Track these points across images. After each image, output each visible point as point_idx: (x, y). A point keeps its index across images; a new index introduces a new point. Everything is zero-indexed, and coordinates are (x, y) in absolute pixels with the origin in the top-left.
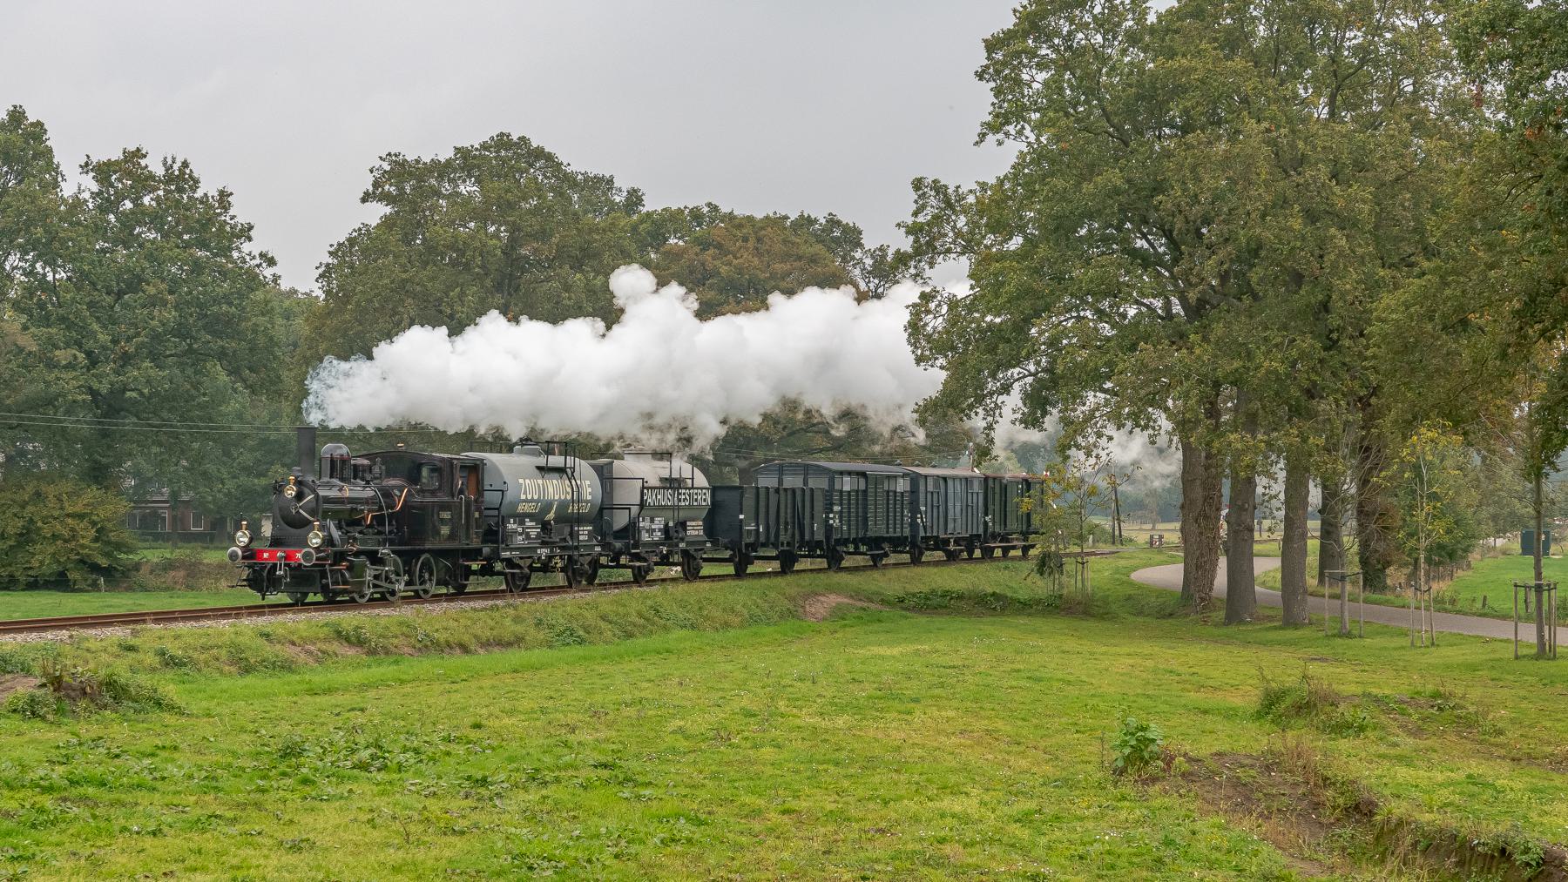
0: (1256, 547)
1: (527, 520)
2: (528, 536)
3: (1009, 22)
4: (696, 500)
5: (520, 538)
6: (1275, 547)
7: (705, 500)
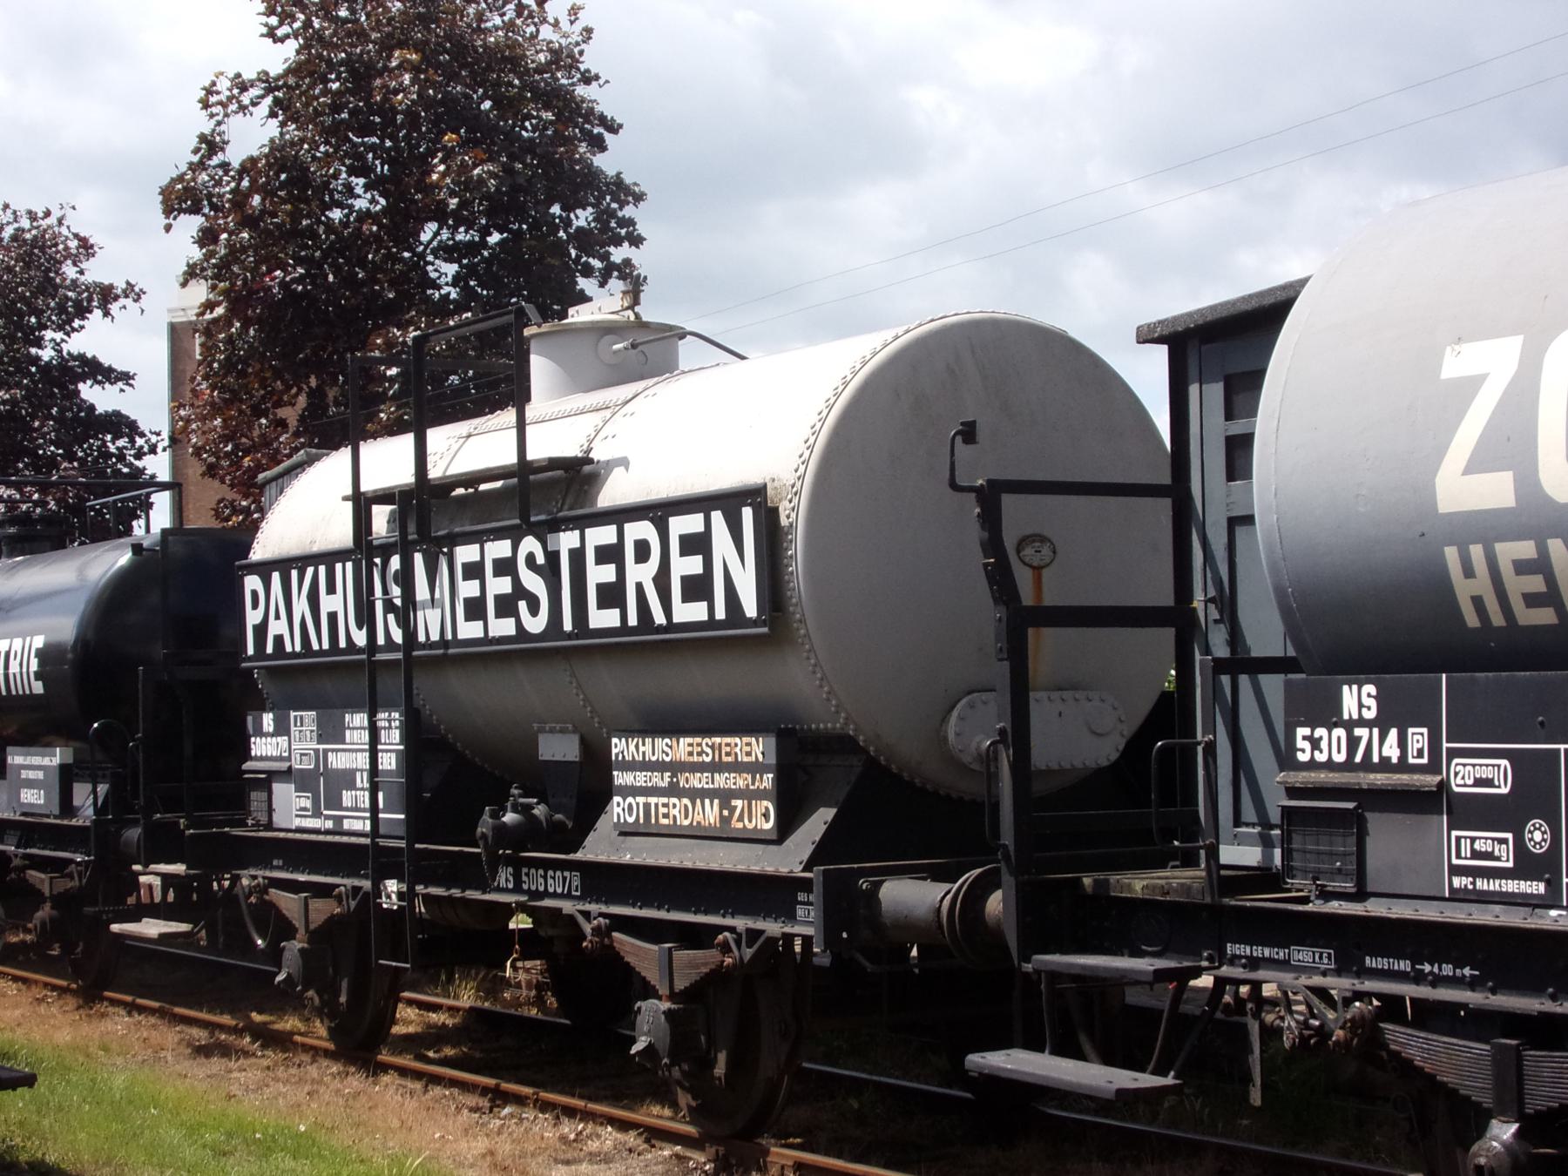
0: (767, 781)
7: (697, 588)
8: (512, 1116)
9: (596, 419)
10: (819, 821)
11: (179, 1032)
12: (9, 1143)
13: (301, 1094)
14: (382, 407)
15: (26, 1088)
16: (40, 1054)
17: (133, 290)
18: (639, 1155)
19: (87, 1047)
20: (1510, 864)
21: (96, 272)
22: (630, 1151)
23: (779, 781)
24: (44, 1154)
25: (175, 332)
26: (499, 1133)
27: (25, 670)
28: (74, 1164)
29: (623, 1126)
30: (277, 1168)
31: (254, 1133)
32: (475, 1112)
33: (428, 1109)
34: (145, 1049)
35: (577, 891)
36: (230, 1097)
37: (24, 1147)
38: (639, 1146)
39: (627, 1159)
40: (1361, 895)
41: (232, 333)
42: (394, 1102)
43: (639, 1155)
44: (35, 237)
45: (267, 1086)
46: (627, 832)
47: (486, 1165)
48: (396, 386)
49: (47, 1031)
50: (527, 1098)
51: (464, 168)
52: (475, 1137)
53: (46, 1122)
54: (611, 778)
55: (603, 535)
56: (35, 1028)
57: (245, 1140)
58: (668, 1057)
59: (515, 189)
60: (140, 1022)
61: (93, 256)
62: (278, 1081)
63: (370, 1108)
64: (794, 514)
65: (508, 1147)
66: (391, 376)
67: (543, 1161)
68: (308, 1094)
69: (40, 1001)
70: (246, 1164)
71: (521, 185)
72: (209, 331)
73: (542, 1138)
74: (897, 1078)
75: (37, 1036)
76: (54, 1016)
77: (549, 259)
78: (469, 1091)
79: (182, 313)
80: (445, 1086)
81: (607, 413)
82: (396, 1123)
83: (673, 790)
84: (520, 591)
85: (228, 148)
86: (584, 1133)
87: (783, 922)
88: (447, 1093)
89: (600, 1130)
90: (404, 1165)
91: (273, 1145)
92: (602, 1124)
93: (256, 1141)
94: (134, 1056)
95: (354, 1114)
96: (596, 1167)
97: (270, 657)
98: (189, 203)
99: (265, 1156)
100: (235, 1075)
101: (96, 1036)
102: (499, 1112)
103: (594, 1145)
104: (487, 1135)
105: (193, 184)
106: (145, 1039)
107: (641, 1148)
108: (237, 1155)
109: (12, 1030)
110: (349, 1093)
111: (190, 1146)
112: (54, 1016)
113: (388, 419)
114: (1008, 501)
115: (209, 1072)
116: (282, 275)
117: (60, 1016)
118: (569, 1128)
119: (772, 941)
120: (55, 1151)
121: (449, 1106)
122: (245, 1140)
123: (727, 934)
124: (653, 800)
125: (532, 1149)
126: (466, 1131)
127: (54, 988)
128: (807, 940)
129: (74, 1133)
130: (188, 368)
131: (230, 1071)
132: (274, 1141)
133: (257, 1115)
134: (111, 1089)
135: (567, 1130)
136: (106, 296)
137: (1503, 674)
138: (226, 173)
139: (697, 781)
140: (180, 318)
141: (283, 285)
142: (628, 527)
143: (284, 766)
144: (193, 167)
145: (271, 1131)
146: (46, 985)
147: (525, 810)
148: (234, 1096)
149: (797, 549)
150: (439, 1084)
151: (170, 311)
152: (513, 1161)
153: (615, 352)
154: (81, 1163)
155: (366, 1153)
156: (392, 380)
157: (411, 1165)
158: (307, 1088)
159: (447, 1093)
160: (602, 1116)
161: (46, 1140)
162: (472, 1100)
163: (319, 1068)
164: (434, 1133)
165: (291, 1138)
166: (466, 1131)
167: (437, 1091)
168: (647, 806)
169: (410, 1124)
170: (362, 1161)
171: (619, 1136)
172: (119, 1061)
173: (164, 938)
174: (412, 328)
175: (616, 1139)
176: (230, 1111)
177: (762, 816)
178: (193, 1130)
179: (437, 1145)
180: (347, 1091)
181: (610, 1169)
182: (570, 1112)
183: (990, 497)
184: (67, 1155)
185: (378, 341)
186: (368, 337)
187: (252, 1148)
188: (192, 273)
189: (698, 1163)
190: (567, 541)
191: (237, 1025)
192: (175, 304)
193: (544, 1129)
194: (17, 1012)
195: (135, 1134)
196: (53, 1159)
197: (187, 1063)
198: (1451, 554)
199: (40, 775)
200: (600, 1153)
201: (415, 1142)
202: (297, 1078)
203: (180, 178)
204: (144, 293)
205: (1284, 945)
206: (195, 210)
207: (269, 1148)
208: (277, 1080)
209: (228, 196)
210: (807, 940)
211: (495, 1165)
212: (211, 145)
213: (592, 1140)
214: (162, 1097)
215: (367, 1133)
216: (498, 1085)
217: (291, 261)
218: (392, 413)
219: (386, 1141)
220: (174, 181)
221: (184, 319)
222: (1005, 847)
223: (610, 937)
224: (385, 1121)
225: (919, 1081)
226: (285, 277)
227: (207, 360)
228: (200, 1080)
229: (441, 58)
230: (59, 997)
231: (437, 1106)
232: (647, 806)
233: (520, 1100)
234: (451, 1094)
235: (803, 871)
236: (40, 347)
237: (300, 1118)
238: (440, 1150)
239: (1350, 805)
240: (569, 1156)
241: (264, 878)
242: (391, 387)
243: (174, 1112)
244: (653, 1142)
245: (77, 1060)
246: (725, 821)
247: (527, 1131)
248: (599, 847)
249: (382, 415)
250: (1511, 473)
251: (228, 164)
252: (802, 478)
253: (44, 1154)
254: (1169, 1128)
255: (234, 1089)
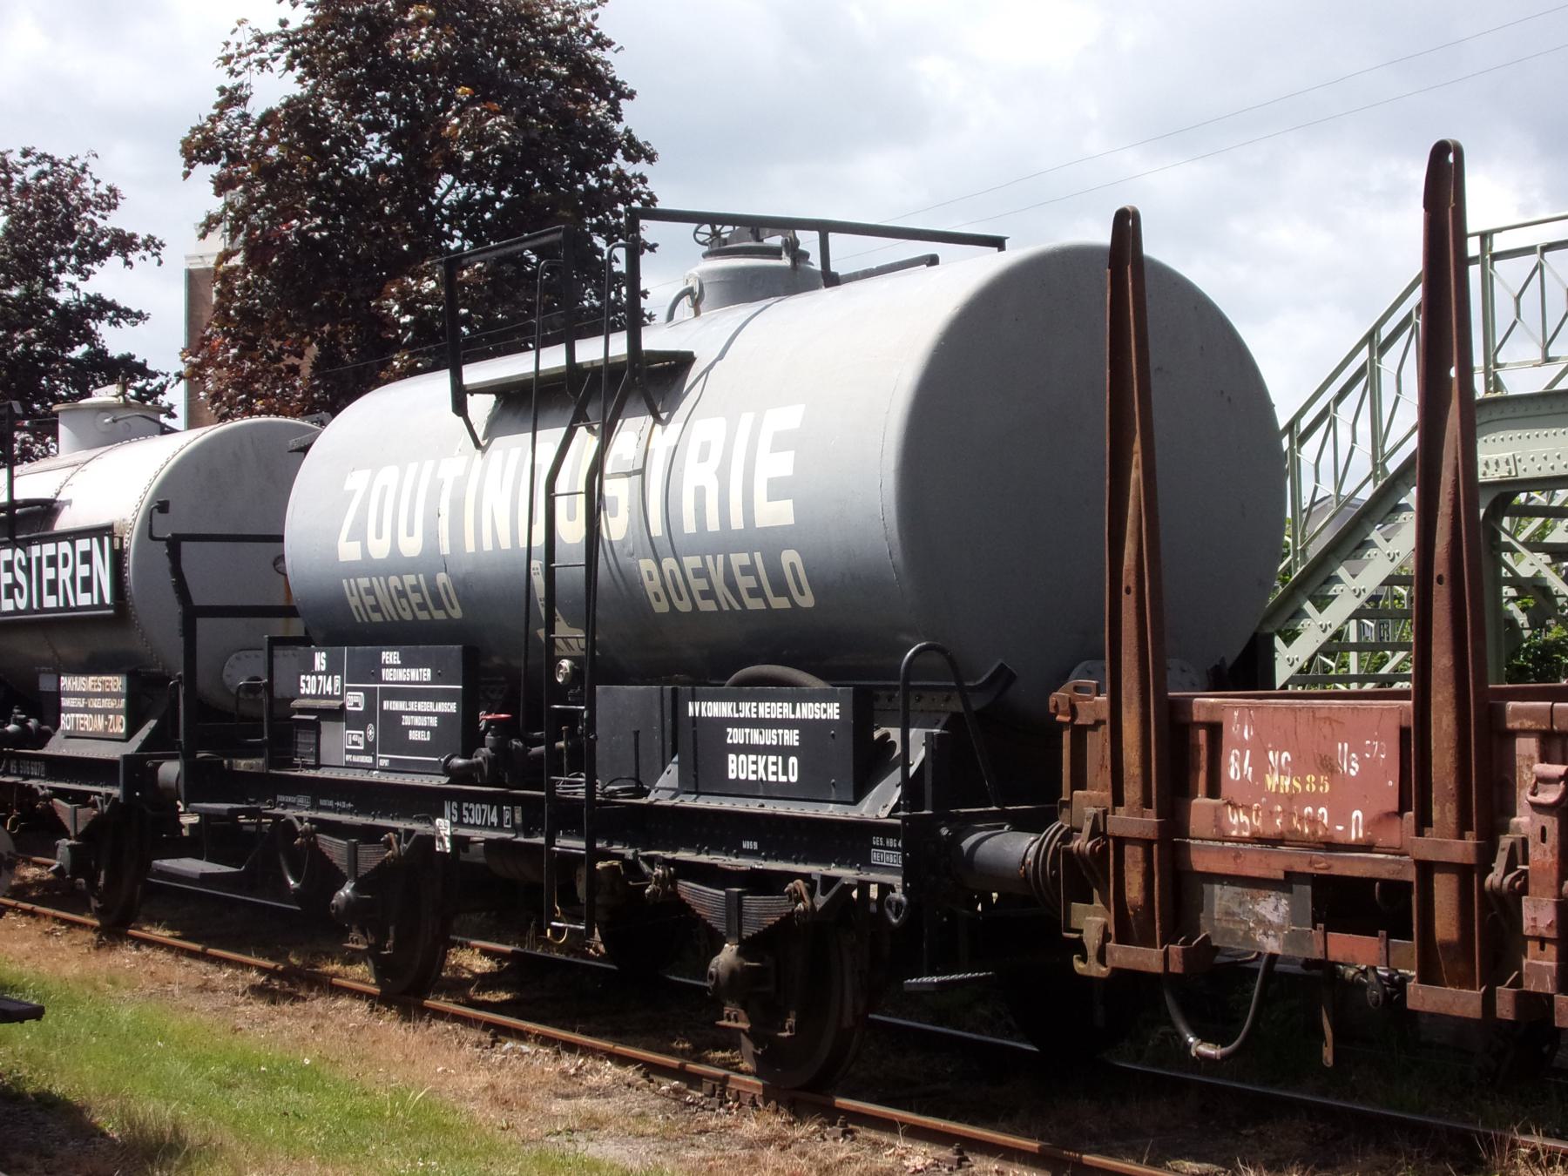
0: (122, 703)
1: (390, 656)
2: (393, 733)
3: (640, 140)
4: (53, 587)
5: (354, 737)
6: (761, 715)
7: (87, 585)
8: (513, 1050)
9: (69, 471)
10: (143, 733)
11: (186, 966)
12: (17, 1075)
13: (306, 1028)
14: (396, 356)
15: (33, 1021)
16: (48, 987)
17: (153, 242)
18: (637, 1089)
19: (95, 979)
20: (362, 748)
21: (114, 221)
22: (629, 1085)
23: (129, 704)
24: (50, 1086)
25: (193, 278)
26: (500, 1068)
27: (385, 590)
28: (80, 1095)
29: (623, 1061)
30: (282, 1101)
31: (259, 1066)
32: (477, 1047)
33: (431, 1043)
34: (153, 983)
35: (508, 823)
36: (236, 1030)
37: (31, 1078)
38: (637, 1081)
39: (625, 1094)
40: (318, 766)
41: (249, 280)
42: (398, 1036)
43: (637, 1089)
44: (53, 184)
45: (273, 1019)
46: (69, 736)
47: (487, 1098)
48: (410, 334)
49: (55, 964)
50: (529, 1033)
51: (478, 120)
52: (477, 1071)
53: (53, 1054)
54: (60, 701)
55: (49, 549)
56: (43, 961)
57: (250, 1073)
58: (70, 873)
59: (530, 142)
60: (147, 956)
61: (115, 208)
62: (283, 1015)
63: (374, 1042)
64: (130, 543)
65: (508, 1081)
66: (405, 324)
67: (543, 1095)
68: (313, 1027)
69: (49, 934)
70: (251, 1097)
71: (534, 139)
72: (226, 277)
73: (543, 1073)
74: (890, 1016)
75: (45, 969)
76: (63, 950)
77: (561, 212)
78: (471, 1026)
79: (199, 260)
80: (448, 1021)
81: (75, 468)
82: (399, 1057)
83: (86, 710)
84: (16, 584)
85: (250, 102)
86: (584, 1068)
87: (859, 869)
88: (450, 1027)
89: (599, 1064)
90: (406, 1097)
91: (277, 1077)
92: (601, 1059)
93: (260, 1073)
94: (141, 989)
95: (358, 1048)
96: (595, 1101)
97: (36, 612)
98: (208, 152)
99: (270, 1088)
100: (242, 1008)
101: (104, 969)
102: (501, 1047)
103: (593, 1080)
104: (489, 1069)
105: (211, 134)
106: (152, 973)
107: (640, 1083)
108: (242, 1087)
109: (21, 963)
110: (354, 1027)
111: (195, 1078)
112: (63, 950)
113: (402, 367)
114: (185, 545)
115: (215, 1006)
116: (299, 224)
117: (68, 950)
118: (569, 1063)
119: (848, 888)
120: (62, 1083)
121: (452, 1041)
122: (250, 1073)
123: (799, 881)
124: (78, 715)
125: (532, 1083)
126: (468, 1065)
127: (63, 921)
128: (885, 889)
129: (81, 1066)
130: (204, 314)
131: (237, 1005)
132: (279, 1073)
133: (262, 1048)
134: (117, 1022)
135: (567, 1065)
136: (124, 243)
137: (357, 648)
138: (246, 124)
139: (95, 704)
140: (198, 265)
141: (300, 233)
142: (78, 542)
143: (337, 703)
144: (212, 119)
145: (276, 1064)
146: (55, 918)
147: (22, 723)
148: (240, 1029)
149: (130, 563)
150: (442, 1019)
151: (187, 258)
152: (515, 1094)
153: (107, 424)
154: (86, 1094)
155: (369, 1087)
156: (405, 327)
157: (414, 1097)
158: (312, 1022)
159: (450, 1027)
160: (601, 1051)
161: (53, 1071)
162: (474, 1035)
163: (324, 1003)
164: (437, 1068)
165: (296, 1071)
166: (468, 1065)
167: (440, 1026)
168: (75, 719)
169: (412, 1058)
170: (365, 1094)
171: (618, 1071)
172: (127, 994)
173: (206, 879)
174: (426, 278)
175: (615, 1074)
176: (235, 1044)
177: (119, 726)
178: (198, 1062)
179: (439, 1079)
180: (351, 1025)
181: (609, 1103)
182: (571, 1047)
183: (174, 544)
184: (73, 1086)
185: (393, 290)
186: (383, 285)
187: (257, 1081)
188: (210, 224)
189: (695, 1098)
190: (35, 551)
191: (276, 966)
192: (193, 252)
193: (545, 1064)
194: (26, 945)
195: (141, 1067)
196: (59, 1091)
197: (194, 997)
198: (344, 581)
199: (791, 737)
200: (599, 1087)
201: (417, 1075)
202: (302, 1012)
203: (201, 129)
204: (163, 246)
205: (294, 795)
206: (214, 159)
207: (274, 1081)
208: (282, 1014)
209: (247, 147)
210: (885, 889)
211: (497, 1099)
212: (232, 98)
213: (592, 1075)
214: (169, 1030)
215: (371, 1067)
216: (682, 1066)
217: (308, 212)
218: (405, 361)
219: (389, 1075)
220: (194, 130)
221: (202, 267)
222: (180, 742)
223: (315, 838)
224: (388, 1054)
225: (911, 1020)
226: (301, 226)
227: (222, 309)
228: (206, 1014)
229: (458, 14)
230: (68, 929)
231: (440, 1040)
232: (75, 719)
233: (521, 1036)
234: (454, 1029)
235: (889, 816)
236: (57, 291)
237: (305, 1051)
238: (442, 1084)
239: (313, 717)
240: (569, 1090)
241: (50, 788)
242: (405, 334)
243: (181, 1045)
244: (652, 1076)
245: (85, 993)
246: (106, 727)
247: (528, 1065)
248: (57, 747)
249: (395, 363)
250: (359, 543)
251: (248, 116)
252: (134, 520)
253: (50, 1086)
254: (1154, 1066)
255: (240, 1022)
